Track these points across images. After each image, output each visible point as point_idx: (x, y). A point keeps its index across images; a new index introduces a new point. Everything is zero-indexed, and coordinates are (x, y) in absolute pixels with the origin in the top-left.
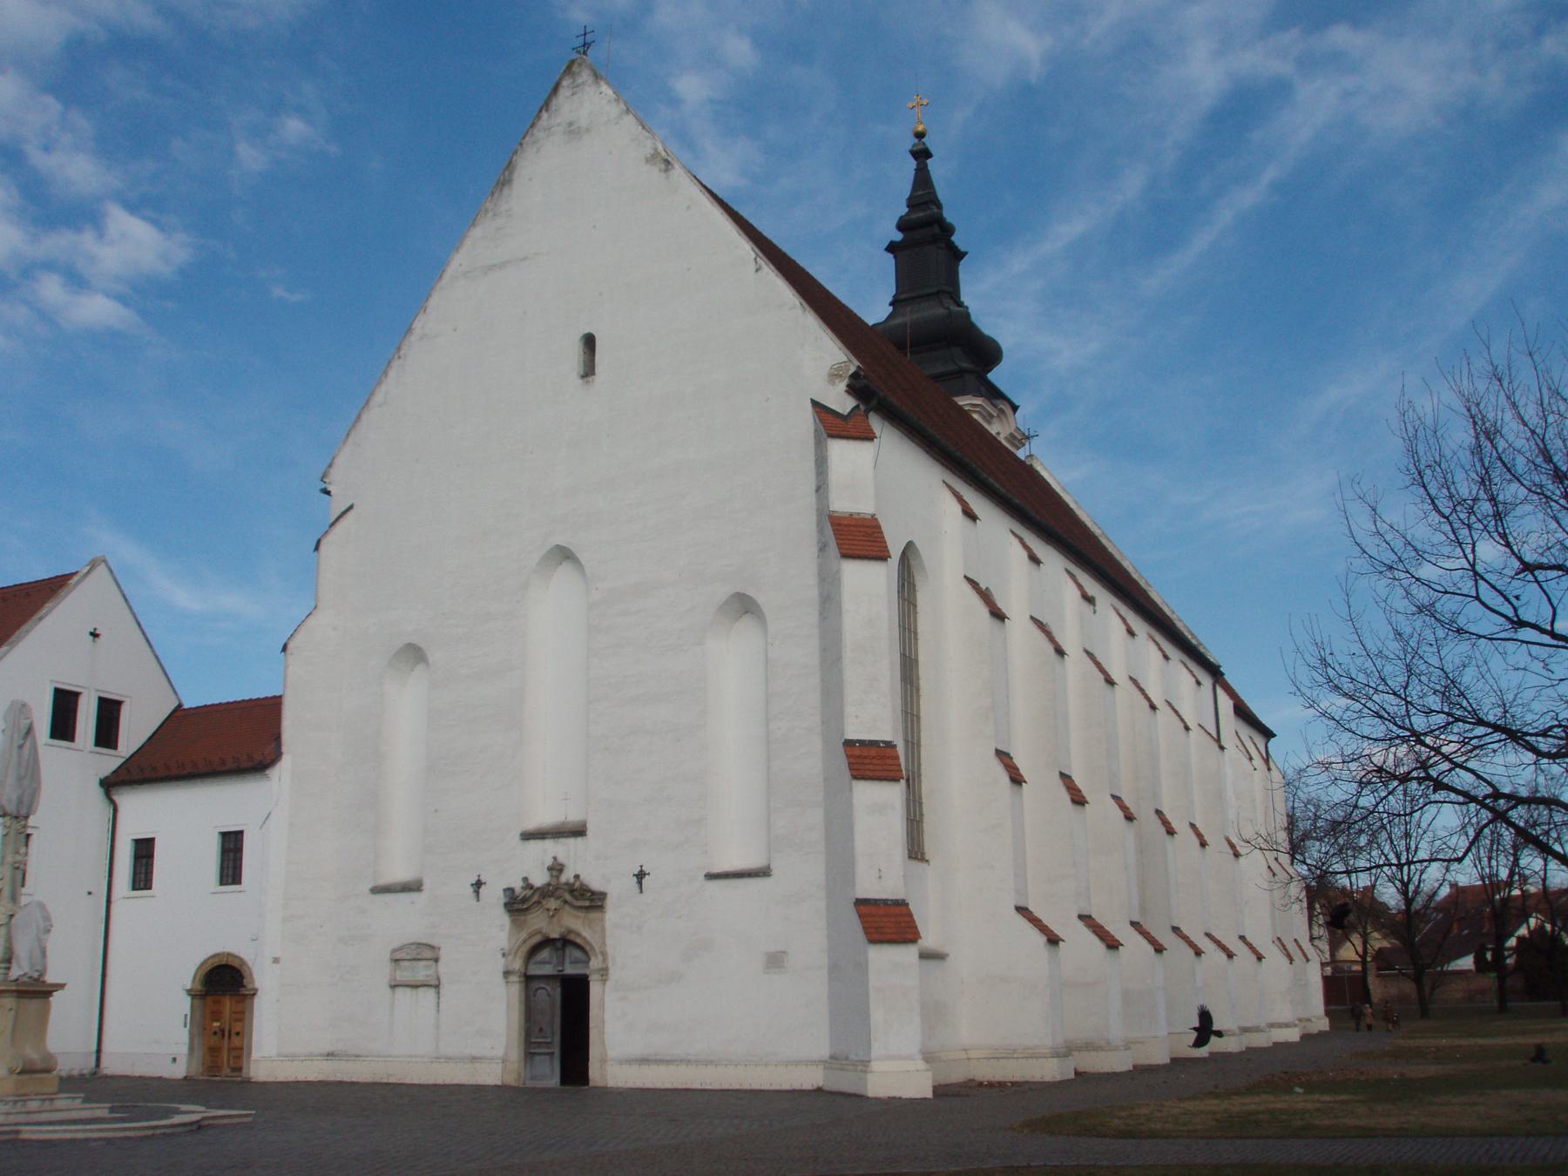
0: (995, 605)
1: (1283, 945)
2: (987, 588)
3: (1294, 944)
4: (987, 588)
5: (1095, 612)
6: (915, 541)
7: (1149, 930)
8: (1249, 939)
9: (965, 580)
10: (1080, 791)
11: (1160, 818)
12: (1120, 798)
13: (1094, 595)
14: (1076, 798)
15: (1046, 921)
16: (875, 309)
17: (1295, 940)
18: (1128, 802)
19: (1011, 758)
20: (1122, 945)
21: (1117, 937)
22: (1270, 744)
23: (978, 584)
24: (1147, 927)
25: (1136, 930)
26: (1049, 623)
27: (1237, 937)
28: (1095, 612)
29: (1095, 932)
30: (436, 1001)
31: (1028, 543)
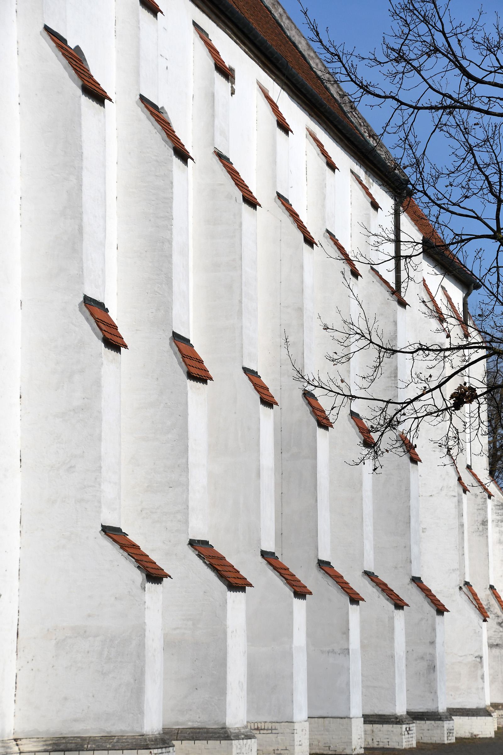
0: (91, 77)
1: (474, 595)
2: (78, 48)
3: (489, 592)
4: (78, 48)
5: (233, 93)
6: (164, 107)
7: (287, 564)
8: (426, 582)
9: (45, 34)
10: (201, 361)
11: (309, 404)
12: (101, 305)
13: (233, 66)
14: (194, 371)
15: (145, 548)
16: (442, 110)
17: (492, 587)
18: (265, 380)
19: (107, 310)
20: (250, 585)
21: (243, 573)
22: (469, 299)
23: (64, 41)
24: (285, 560)
25: (270, 563)
26: (166, 109)
27: (408, 580)
28: (233, 93)
29: (212, 567)
30: (275, 721)
31: (215, 43)
